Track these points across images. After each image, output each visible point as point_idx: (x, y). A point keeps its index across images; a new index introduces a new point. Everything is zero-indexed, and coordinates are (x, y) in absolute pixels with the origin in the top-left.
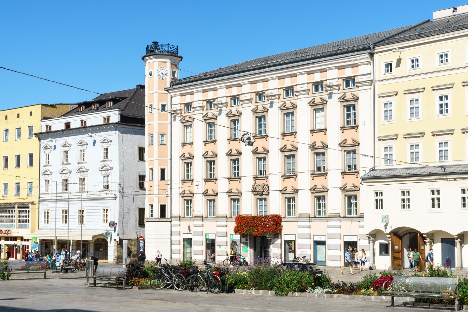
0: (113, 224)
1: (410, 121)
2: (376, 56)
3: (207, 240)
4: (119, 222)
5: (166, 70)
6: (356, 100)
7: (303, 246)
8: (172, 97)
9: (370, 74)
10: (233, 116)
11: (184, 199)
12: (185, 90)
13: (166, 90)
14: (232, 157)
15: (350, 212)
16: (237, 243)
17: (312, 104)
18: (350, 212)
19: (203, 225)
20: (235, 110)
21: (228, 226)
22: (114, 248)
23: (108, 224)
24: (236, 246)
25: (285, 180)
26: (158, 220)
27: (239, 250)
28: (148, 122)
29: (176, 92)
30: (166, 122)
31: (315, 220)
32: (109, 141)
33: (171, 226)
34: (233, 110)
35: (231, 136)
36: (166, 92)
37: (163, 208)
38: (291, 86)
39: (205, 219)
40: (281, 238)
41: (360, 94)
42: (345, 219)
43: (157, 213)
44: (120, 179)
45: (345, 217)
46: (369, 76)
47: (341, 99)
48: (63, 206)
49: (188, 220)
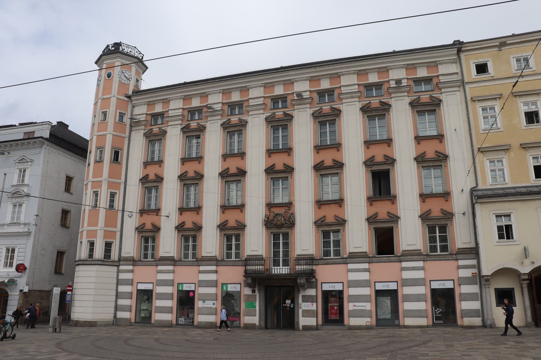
0: (21, 268)
1: (528, 128)
2: (462, 55)
3: (179, 291)
4: (30, 266)
5: (129, 74)
6: (437, 104)
7: (205, 298)
8: (133, 107)
9: (457, 73)
10: (232, 126)
11: (141, 235)
12: (274, 78)
13: (126, 97)
14: (229, 178)
15: (146, 256)
16: (234, 296)
17: (365, 110)
18: (146, 256)
19: (174, 270)
20: (238, 119)
21: (218, 272)
22: (18, 302)
23: (13, 269)
24: (233, 301)
25: (373, 203)
26: (101, 263)
27: (238, 307)
28: (125, 134)
29: (142, 99)
30: (124, 135)
31: (378, 261)
32: (29, 160)
33: (119, 272)
34: (232, 120)
35: (148, 159)
36: (126, 99)
37: (108, 246)
38: (240, 101)
39: (178, 263)
40: (316, 288)
41: (392, 102)
42: (224, 263)
43: (99, 253)
44: (38, 209)
45: (180, 260)
46: (456, 76)
47: (414, 103)
48: (9, 243)
49: (146, 264)
